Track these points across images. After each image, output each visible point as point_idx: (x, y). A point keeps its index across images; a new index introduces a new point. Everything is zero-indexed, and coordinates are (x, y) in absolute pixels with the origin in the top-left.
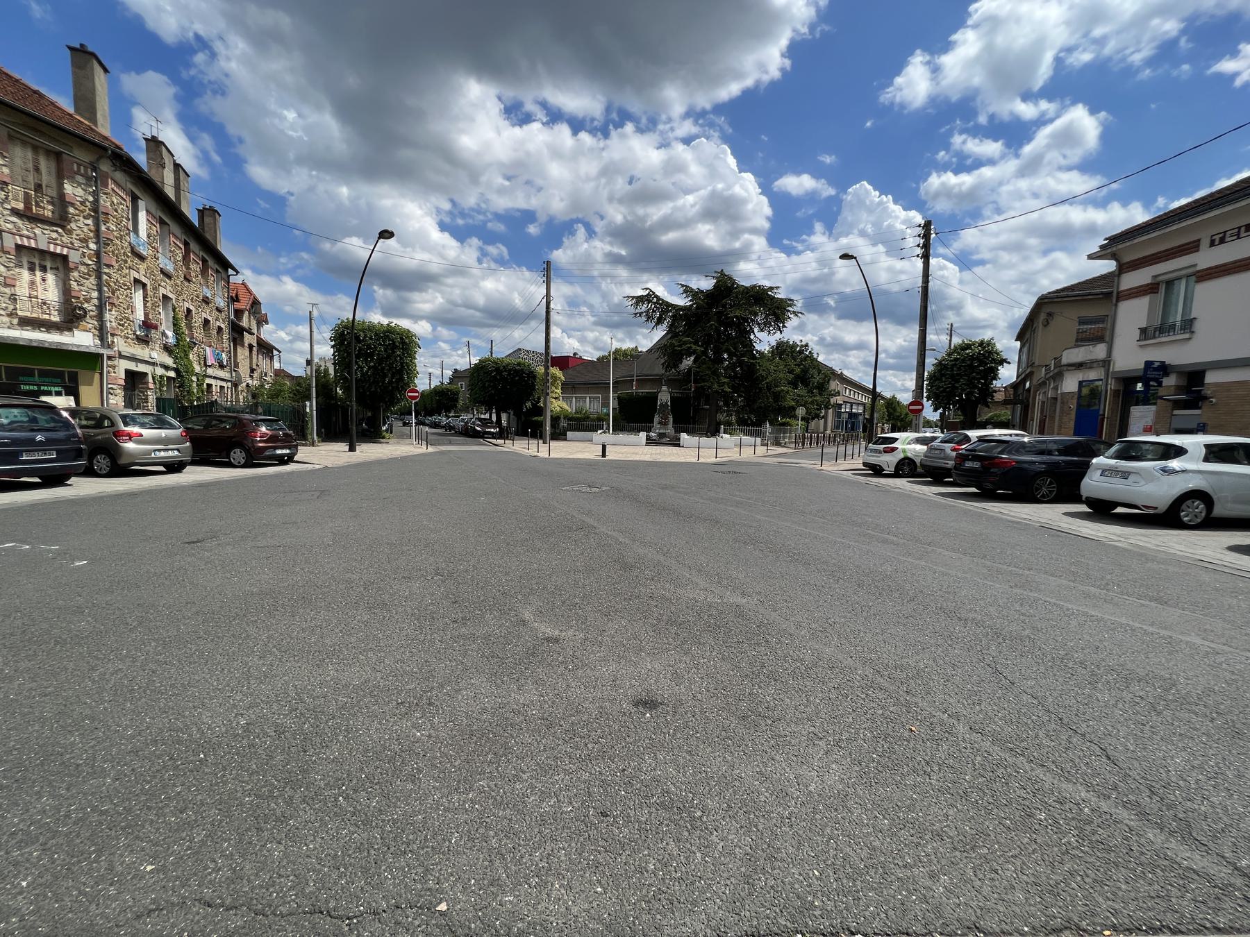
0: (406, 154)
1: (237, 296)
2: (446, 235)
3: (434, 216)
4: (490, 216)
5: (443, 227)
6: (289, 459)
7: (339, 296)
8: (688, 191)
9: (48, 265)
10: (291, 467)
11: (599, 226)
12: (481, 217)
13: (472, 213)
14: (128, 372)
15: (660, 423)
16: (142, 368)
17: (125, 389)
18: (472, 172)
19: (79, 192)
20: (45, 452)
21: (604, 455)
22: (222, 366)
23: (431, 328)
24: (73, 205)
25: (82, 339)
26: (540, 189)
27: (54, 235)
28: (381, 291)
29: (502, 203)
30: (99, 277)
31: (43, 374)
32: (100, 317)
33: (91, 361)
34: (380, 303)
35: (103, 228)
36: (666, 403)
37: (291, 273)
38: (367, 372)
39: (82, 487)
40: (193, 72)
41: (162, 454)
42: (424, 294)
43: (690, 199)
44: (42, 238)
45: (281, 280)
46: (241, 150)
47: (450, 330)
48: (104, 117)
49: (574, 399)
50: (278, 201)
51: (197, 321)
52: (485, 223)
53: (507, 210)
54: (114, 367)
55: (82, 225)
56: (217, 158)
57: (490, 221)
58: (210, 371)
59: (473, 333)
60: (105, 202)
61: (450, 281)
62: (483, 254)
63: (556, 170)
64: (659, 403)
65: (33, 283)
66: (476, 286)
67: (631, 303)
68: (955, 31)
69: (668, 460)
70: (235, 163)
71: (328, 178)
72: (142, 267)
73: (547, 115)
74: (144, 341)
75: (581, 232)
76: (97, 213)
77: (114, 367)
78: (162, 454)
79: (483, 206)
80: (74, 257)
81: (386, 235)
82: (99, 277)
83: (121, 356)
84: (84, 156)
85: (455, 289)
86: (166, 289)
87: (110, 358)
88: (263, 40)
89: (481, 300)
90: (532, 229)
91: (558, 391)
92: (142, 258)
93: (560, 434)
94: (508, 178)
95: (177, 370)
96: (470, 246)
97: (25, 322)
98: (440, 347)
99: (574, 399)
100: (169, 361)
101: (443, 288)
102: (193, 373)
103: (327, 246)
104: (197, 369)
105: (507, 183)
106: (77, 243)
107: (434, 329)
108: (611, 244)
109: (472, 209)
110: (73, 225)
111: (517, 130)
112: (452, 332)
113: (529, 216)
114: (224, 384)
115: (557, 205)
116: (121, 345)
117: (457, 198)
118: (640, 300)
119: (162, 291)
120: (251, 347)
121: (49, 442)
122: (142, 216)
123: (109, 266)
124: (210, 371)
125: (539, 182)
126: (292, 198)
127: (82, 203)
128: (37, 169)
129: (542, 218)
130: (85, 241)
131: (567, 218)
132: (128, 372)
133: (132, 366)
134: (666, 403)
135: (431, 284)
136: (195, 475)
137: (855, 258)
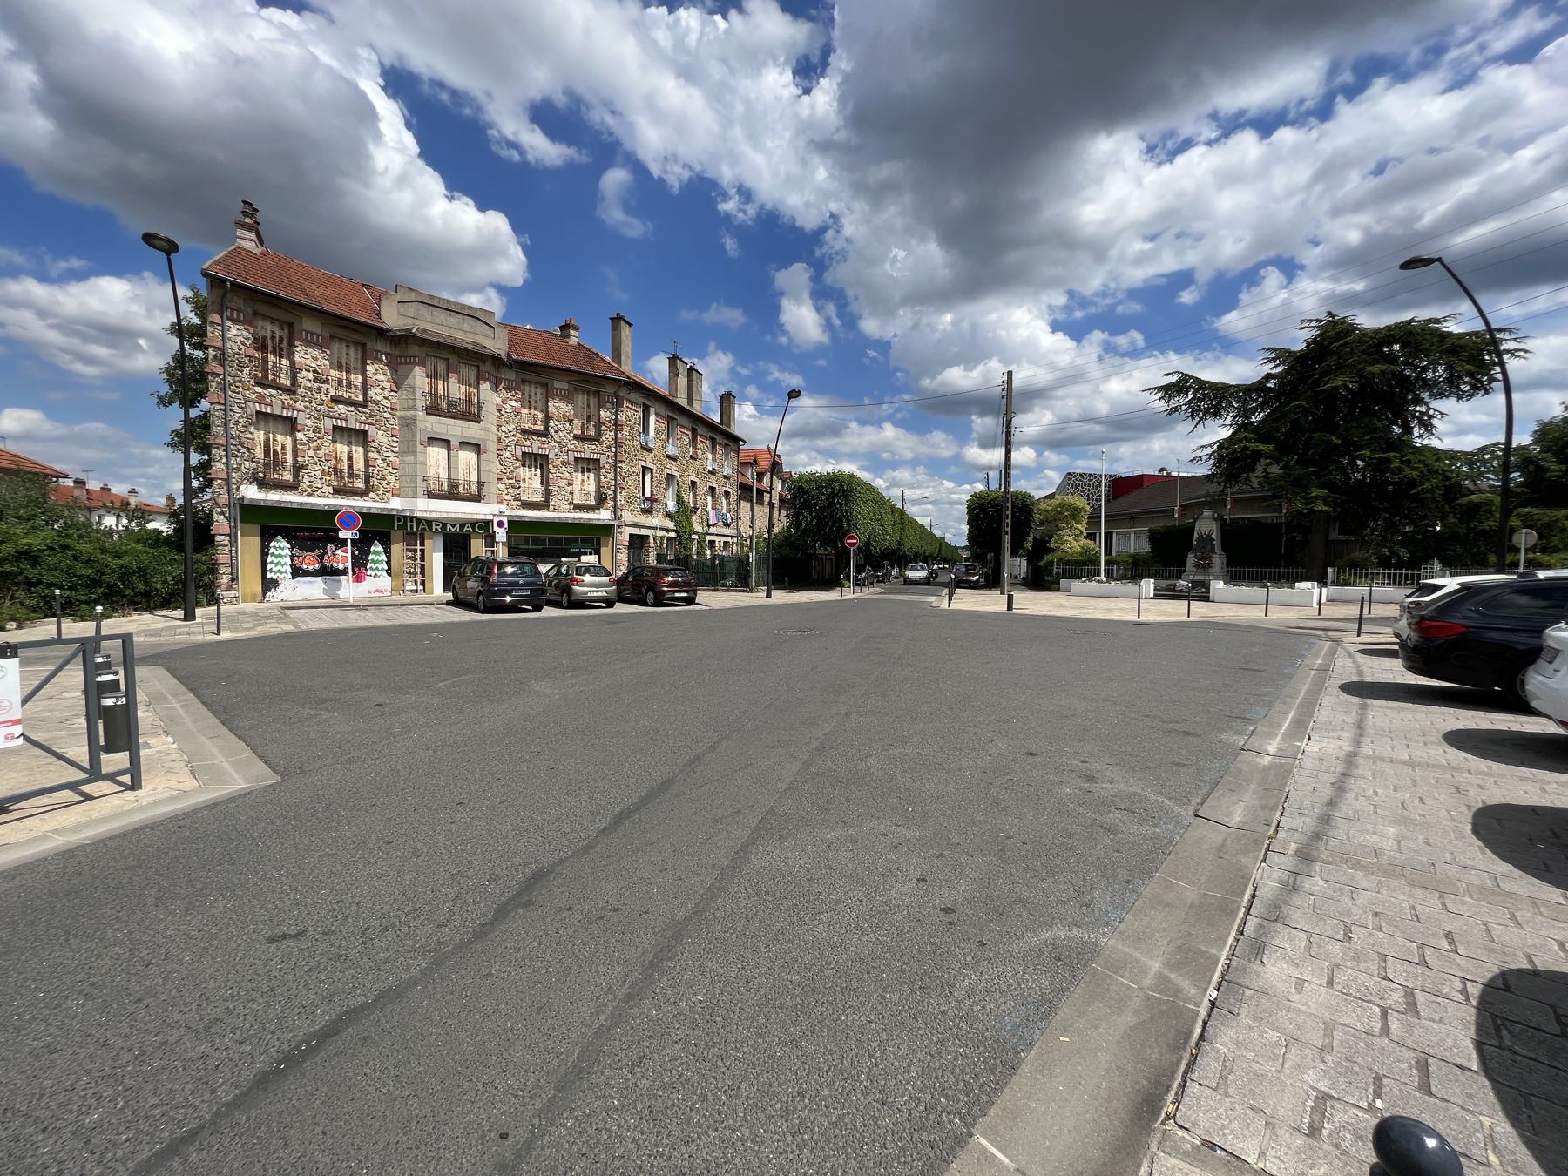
0: (1013, 257)
1: (756, 461)
2: (1060, 336)
3: (1046, 316)
4: (1120, 296)
5: (1055, 327)
6: (690, 601)
7: (935, 433)
8: (1511, 146)
9: (591, 467)
10: (694, 607)
11: (1311, 256)
12: (1108, 301)
13: (1095, 299)
14: (631, 536)
15: (1197, 566)
16: (644, 532)
17: (629, 547)
18: (1098, 249)
19: (608, 414)
20: (524, 590)
21: (1010, 607)
22: (727, 525)
23: (1035, 454)
24: (604, 424)
25: (604, 515)
26: (1199, 238)
27: (594, 447)
28: (979, 420)
29: (1137, 275)
30: (616, 471)
31: (584, 540)
32: (615, 499)
33: (607, 529)
34: (977, 433)
35: (619, 436)
36: (1209, 536)
37: (890, 418)
38: (811, 522)
39: (548, 612)
40: (825, 249)
41: (595, 594)
42: (1030, 415)
43: (1527, 154)
44: (587, 450)
45: (881, 428)
46: (854, 308)
47: (1059, 453)
48: (627, 357)
49: (1132, 535)
50: (884, 346)
51: (702, 489)
52: (1112, 307)
53: (1145, 281)
54: (621, 533)
55: (608, 437)
56: (837, 322)
57: (1120, 302)
58: (713, 530)
59: (1090, 453)
60: (622, 417)
61: (1060, 393)
62: (1109, 348)
63: (1227, 202)
64: (1196, 536)
65: (583, 480)
66: (1097, 391)
67: (1157, 397)
68: (653, 177)
69: (1100, 616)
70: (851, 322)
71: (931, 309)
72: (650, 457)
73: (1218, 127)
74: (648, 512)
75: (1273, 277)
76: (617, 426)
77: (621, 533)
78: (595, 594)
79: (1112, 285)
80: (603, 459)
81: (794, 394)
82: (616, 471)
83: (626, 525)
84: (610, 389)
85: (1068, 403)
86: (672, 468)
87: (619, 527)
88: (877, 195)
89: (1103, 409)
90: (1187, 297)
91: (1079, 526)
92: (650, 450)
93: (1053, 583)
94: (1152, 238)
95: (676, 531)
96: (1091, 343)
97: (578, 507)
98: (1046, 477)
99: (1132, 535)
100: (671, 525)
101: (1053, 402)
102: (692, 532)
103: (926, 382)
104: (698, 528)
105: (1148, 246)
106: (605, 450)
107: (1039, 454)
108: (1334, 279)
109: (1096, 294)
110: (604, 438)
111: (1167, 169)
112: (1063, 456)
113: (1183, 279)
114: (729, 539)
115: (1230, 249)
116: (627, 516)
117: (1075, 286)
118: (1167, 391)
119: (667, 471)
120: (771, 505)
121: (525, 584)
122: (652, 418)
123: (621, 461)
124: (713, 530)
125: (1198, 226)
126: (896, 339)
127: (609, 422)
128: (588, 406)
129: (1203, 277)
130: (609, 447)
131: (1250, 264)
132: (631, 536)
133: (635, 531)
134: (1209, 536)
135: (1036, 401)
136: (621, 608)
137: (1439, 260)
